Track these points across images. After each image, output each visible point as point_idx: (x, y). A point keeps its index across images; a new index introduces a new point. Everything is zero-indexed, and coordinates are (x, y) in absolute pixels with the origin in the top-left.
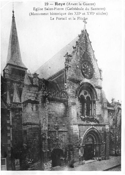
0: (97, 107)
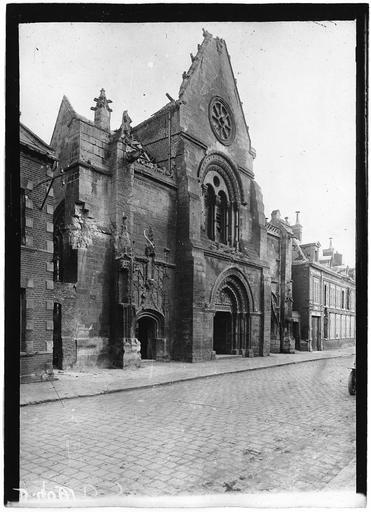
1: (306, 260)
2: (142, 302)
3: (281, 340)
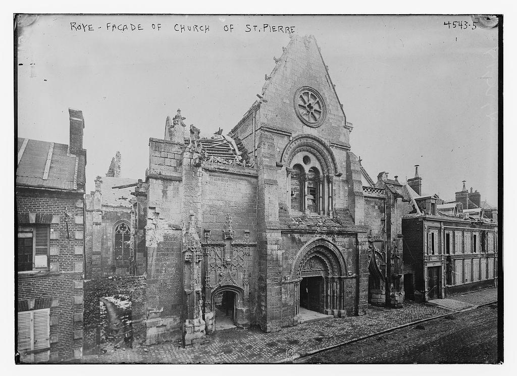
0: (335, 190)
1: (419, 214)
2: (220, 281)
3: (387, 294)
